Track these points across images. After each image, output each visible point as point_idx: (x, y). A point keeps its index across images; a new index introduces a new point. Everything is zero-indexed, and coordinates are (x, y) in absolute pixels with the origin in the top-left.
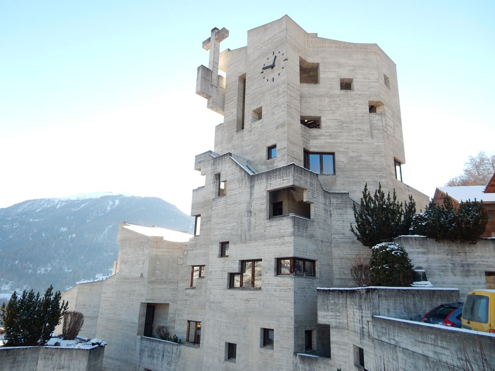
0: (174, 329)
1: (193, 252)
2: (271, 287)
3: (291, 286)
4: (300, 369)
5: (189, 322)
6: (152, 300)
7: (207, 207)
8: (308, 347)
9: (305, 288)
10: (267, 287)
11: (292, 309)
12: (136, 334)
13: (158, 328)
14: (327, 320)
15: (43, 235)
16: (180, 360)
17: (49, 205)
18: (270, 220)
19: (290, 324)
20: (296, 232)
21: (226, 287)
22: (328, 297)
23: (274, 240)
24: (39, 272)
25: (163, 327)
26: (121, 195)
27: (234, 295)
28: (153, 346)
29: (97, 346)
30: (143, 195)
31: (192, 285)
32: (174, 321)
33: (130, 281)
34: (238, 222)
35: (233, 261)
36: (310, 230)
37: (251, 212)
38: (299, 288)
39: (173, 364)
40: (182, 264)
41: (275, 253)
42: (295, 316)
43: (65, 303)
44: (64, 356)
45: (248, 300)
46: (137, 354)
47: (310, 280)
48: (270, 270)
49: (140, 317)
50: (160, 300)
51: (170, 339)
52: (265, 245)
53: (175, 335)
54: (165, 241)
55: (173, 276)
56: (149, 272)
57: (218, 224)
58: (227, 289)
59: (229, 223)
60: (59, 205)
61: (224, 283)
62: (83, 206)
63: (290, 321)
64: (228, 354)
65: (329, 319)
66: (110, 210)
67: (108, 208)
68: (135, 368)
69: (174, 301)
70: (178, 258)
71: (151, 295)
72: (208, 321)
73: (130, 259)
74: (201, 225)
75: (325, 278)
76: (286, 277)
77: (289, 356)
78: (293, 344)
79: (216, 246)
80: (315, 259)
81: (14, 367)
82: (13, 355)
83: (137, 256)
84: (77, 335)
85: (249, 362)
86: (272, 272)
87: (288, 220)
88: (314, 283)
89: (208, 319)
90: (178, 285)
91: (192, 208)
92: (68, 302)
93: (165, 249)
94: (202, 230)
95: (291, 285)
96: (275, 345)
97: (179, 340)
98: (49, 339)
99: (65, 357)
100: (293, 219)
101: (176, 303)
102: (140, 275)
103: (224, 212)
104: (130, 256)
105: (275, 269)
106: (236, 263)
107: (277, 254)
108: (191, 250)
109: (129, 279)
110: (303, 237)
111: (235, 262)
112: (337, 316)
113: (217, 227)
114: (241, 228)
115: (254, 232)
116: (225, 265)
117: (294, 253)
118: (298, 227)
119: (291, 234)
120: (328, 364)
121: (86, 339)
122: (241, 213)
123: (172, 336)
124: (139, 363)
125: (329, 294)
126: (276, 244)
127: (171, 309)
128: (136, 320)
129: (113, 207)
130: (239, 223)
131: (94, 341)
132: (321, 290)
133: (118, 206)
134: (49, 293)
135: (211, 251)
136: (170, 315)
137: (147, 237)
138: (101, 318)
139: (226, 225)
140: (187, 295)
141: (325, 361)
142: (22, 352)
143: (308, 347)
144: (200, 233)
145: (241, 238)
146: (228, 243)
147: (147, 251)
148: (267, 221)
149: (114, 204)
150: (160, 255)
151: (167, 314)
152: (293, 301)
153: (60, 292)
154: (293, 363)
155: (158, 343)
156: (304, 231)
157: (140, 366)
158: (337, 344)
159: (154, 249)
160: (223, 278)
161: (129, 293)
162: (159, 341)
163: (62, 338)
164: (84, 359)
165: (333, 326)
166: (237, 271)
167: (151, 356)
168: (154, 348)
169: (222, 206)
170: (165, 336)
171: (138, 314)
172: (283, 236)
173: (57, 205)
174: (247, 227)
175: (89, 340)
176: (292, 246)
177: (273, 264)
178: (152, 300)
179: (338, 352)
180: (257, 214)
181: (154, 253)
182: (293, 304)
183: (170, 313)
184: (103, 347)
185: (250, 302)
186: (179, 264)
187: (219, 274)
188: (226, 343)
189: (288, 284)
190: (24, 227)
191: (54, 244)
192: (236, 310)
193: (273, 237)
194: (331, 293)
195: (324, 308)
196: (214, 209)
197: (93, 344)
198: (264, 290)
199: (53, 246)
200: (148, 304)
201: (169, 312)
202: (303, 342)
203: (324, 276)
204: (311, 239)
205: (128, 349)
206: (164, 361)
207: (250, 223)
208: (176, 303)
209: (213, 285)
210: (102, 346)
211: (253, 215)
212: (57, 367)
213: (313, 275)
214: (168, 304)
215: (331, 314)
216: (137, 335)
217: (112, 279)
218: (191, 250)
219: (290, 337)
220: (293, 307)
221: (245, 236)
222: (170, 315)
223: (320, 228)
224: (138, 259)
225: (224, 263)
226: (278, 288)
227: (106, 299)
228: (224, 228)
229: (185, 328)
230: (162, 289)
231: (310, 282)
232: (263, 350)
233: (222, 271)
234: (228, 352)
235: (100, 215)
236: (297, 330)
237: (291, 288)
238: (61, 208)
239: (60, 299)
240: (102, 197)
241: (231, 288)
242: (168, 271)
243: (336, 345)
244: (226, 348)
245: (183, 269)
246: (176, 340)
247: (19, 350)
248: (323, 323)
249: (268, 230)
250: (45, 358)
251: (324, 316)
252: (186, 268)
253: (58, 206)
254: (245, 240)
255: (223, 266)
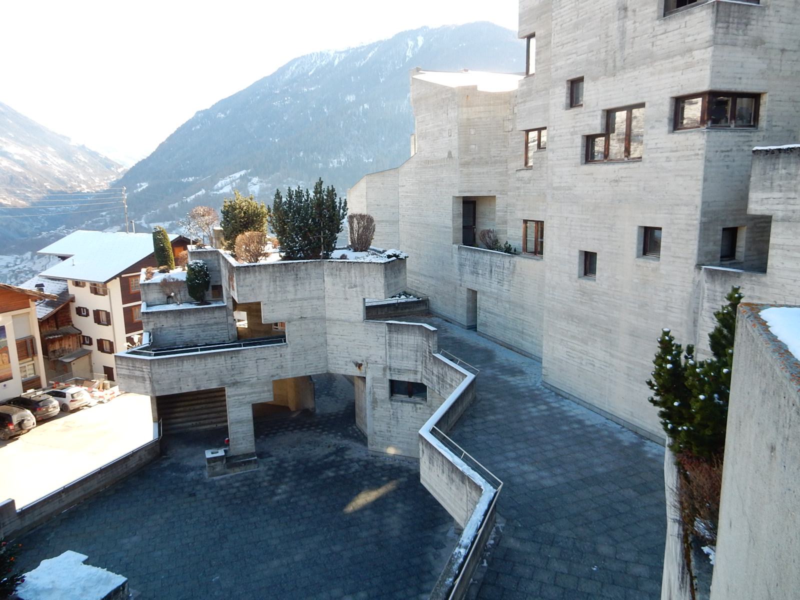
0: (506, 234)
1: (525, 105)
2: (660, 155)
3: (699, 149)
4: (706, 291)
5: (526, 222)
6: (469, 191)
7: (546, 15)
8: (728, 254)
9: (731, 150)
10: (652, 155)
11: (698, 190)
12: (452, 242)
13: (481, 233)
14: (768, 207)
15: (325, 110)
16: (516, 277)
17: (324, 62)
18: (665, 20)
19: (694, 217)
20: (720, 36)
21: (579, 161)
22: (774, 164)
23: (671, 60)
24: (331, 165)
25: (489, 231)
26: (425, 27)
27: (592, 174)
28: (476, 259)
29: (394, 258)
30: (460, 22)
31: (526, 163)
32: (505, 222)
33: (434, 165)
34: (600, 36)
35: (592, 114)
36: (755, 29)
37: (625, 9)
38: (717, 152)
39: (505, 282)
40: (512, 130)
41: (672, 87)
42: (703, 203)
43: (343, 202)
44: (353, 271)
45: (616, 181)
46: (456, 270)
47: (743, 134)
48: (661, 121)
49: (454, 218)
50: (481, 191)
51: (500, 249)
52: (652, 74)
53: (507, 243)
54: (480, 92)
55: (499, 152)
56: (459, 149)
57: (563, 45)
58: (582, 164)
59: (583, 41)
60: (337, 59)
61: (576, 155)
62: (370, 55)
63: (693, 213)
64: (583, 269)
65: (773, 204)
66: (411, 56)
67: (407, 54)
68: (456, 288)
69: (503, 192)
70: (504, 120)
71: (466, 184)
72: (551, 219)
73: (430, 131)
74: (537, 54)
75: (780, 128)
76: (691, 132)
77: (687, 270)
78: (696, 252)
79: (560, 88)
80: (762, 91)
81: (298, 285)
82: (293, 270)
83: (440, 123)
84: (370, 245)
85: (618, 280)
86: (665, 125)
87: (704, 13)
88: (752, 141)
89: (551, 216)
90: (507, 165)
91: (520, 24)
92: (345, 200)
93: (482, 108)
94: (540, 63)
95: (699, 147)
96: (662, 253)
97: (513, 250)
98: (332, 251)
99: (355, 273)
100: (715, 7)
101: (506, 194)
102: (446, 155)
103: (573, 18)
104: (430, 125)
105: (670, 120)
106: (597, 115)
107: (675, 89)
108: (521, 103)
109: (432, 162)
110: (735, 45)
111: (595, 113)
112: (790, 198)
113: (562, 51)
114: (605, 45)
115: (630, 51)
116: (576, 123)
117: (711, 81)
118: (725, 25)
119: (707, 42)
120: (759, 283)
121: (381, 250)
122: (607, 14)
123: (502, 244)
124: (459, 282)
125: (778, 157)
126: (675, 69)
127: (500, 203)
128: (449, 222)
129: (416, 49)
130: (603, 36)
131: (390, 252)
132: (761, 151)
133: (422, 47)
134: (318, 189)
135: (552, 99)
136: (499, 214)
137: (451, 89)
138: (403, 222)
139: (579, 45)
140: (519, 180)
141: (754, 278)
142: (303, 268)
143: (728, 254)
144: (536, 69)
145: (606, 67)
146: (581, 79)
147: (453, 114)
148: (657, 22)
149: (416, 45)
150: (473, 119)
151: (495, 213)
152: (701, 177)
153: (334, 187)
154: (694, 281)
155: (482, 254)
156: (741, 32)
157: (461, 286)
158: (782, 249)
159: (465, 109)
160: (574, 145)
161: (435, 183)
162: (484, 251)
163: (352, 250)
164: (379, 276)
165: (779, 218)
166: (598, 132)
167: (475, 273)
168: (478, 261)
169: (571, 6)
170: (493, 245)
171: (451, 214)
172: (690, 50)
173: (334, 61)
174: (617, 42)
175: (384, 251)
176: (708, 67)
177: (666, 109)
178: (469, 191)
179: (783, 263)
180: (637, 10)
181: (465, 116)
182: (701, 183)
183: (499, 211)
184: (403, 261)
185: (620, 184)
186: (507, 130)
187: (567, 139)
188: (580, 251)
189: (693, 145)
190: (298, 102)
191: (342, 122)
192: (596, 199)
193: (669, 56)
194: (782, 155)
195: (763, 185)
196: (556, 15)
197: (389, 257)
198: (648, 161)
199: (342, 125)
200: (464, 197)
201: (497, 209)
202: (716, 247)
203: (778, 124)
204: (756, 48)
205: (443, 263)
206: (493, 279)
207: (623, 33)
208: (506, 194)
209: (557, 160)
210: (402, 259)
211: (630, 13)
212: (348, 286)
213: (752, 124)
214: (495, 196)
215: (777, 195)
216: (453, 244)
217: (409, 165)
218: (521, 103)
219: (691, 240)
220: (701, 187)
221: (614, 61)
222: (498, 213)
223: (780, 21)
224: (442, 129)
225: (574, 119)
226: (674, 154)
227: (406, 194)
228: (574, 51)
229: (521, 233)
230: (483, 173)
231: (742, 139)
232: (642, 261)
233: (572, 134)
234: (583, 266)
235: (398, 67)
236: (705, 228)
237: (700, 152)
238: (339, 63)
239: (336, 196)
240: (396, 35)
241: (590, 161)
242: (489, 144)
243: (779, 251)
244: (580, 258)
245: (514, 138)
246: (508, 250)
247: (299, 265)
248: (758, 213)
249: (658, 43)
250: (332, 274)
251: (762, 200)
252: (519, 137)
253: (336, 62)
254: (612, 69)
255: (574, 125)
